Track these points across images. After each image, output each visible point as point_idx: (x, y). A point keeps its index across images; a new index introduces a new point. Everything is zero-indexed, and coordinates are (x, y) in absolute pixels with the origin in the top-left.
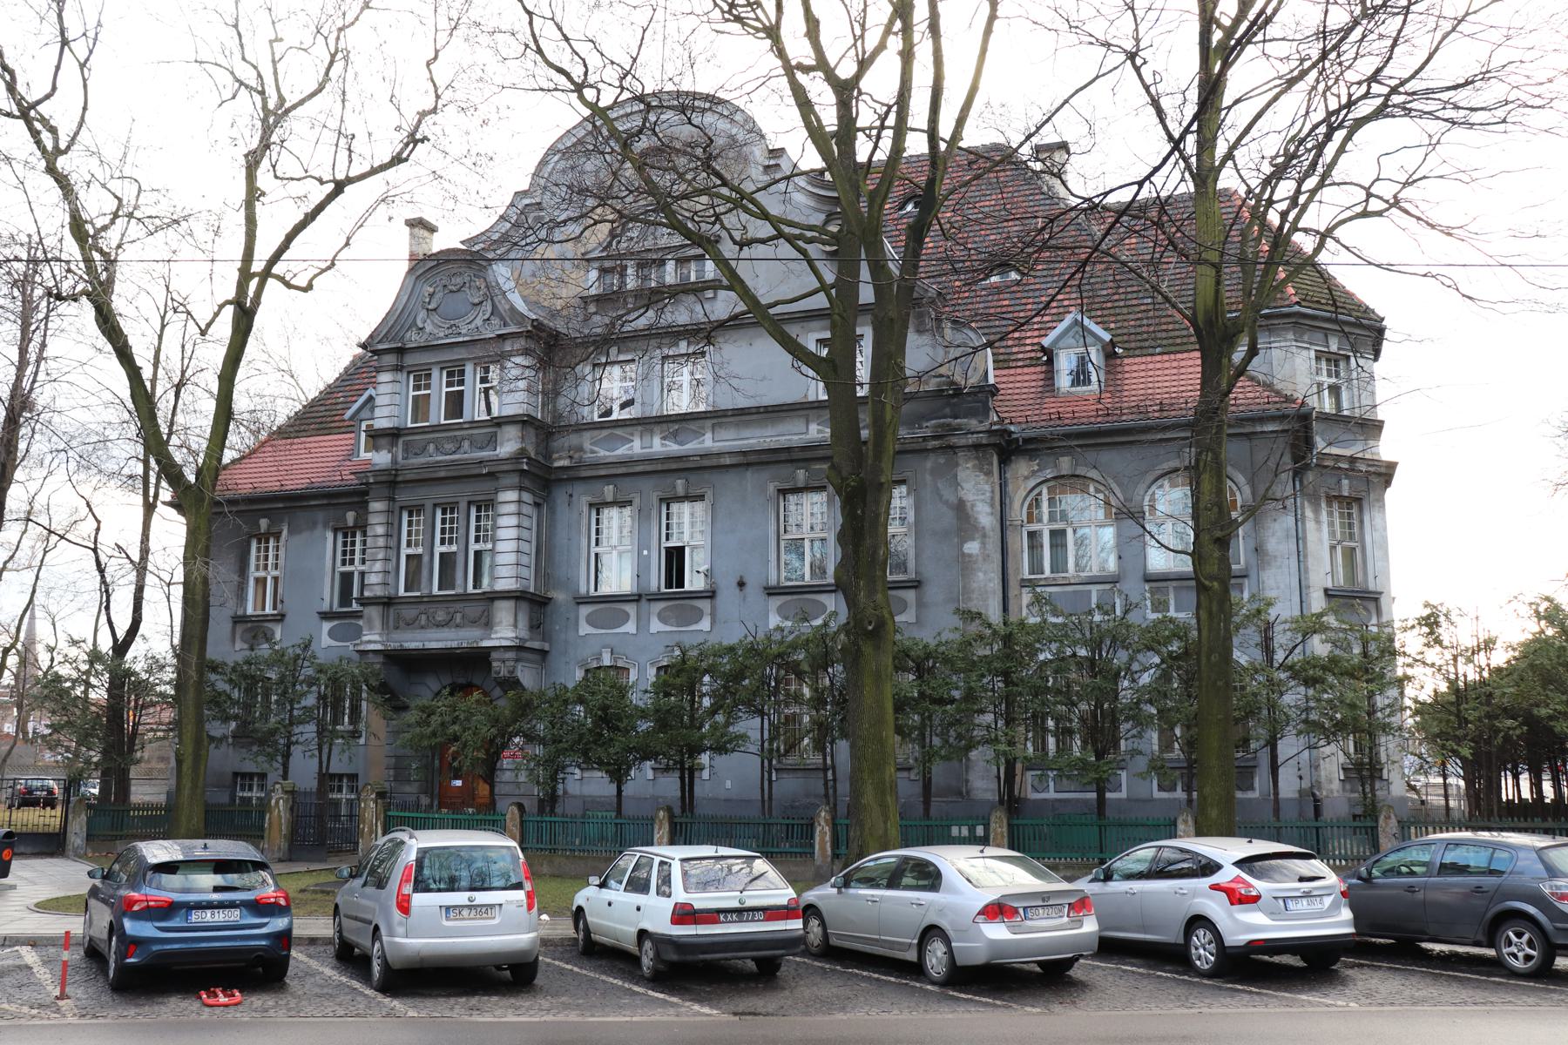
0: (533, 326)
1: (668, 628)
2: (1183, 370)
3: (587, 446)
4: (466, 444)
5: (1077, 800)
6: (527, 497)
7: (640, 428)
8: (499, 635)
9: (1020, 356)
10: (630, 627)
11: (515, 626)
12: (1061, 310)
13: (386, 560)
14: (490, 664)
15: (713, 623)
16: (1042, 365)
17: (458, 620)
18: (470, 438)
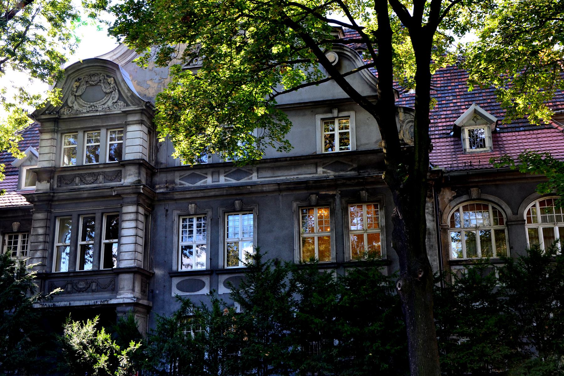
0: (146, 106)
2: (540, 139)
3: (178, 181)
4: (101, 178)
6: (141, 210)
7: (212, 170)
8: (122, 296)
9: (437, 132)
10: (205, 291)
11: (133, 290)
12: (456, 108)
13: (44, 250)
16: (451, 137)
17: (94, 287)
18: (104, 173)
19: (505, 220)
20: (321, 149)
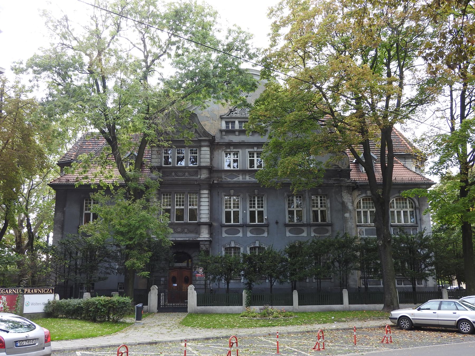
1: (254, 235)
3: (223, 177)
4: (187, 174)
5: (376, 288)
8: (203, 236)
10: (240, 235)
14: (200, 245)
15: (268, 234)
19: (414, 207)
20: (248, 167)
